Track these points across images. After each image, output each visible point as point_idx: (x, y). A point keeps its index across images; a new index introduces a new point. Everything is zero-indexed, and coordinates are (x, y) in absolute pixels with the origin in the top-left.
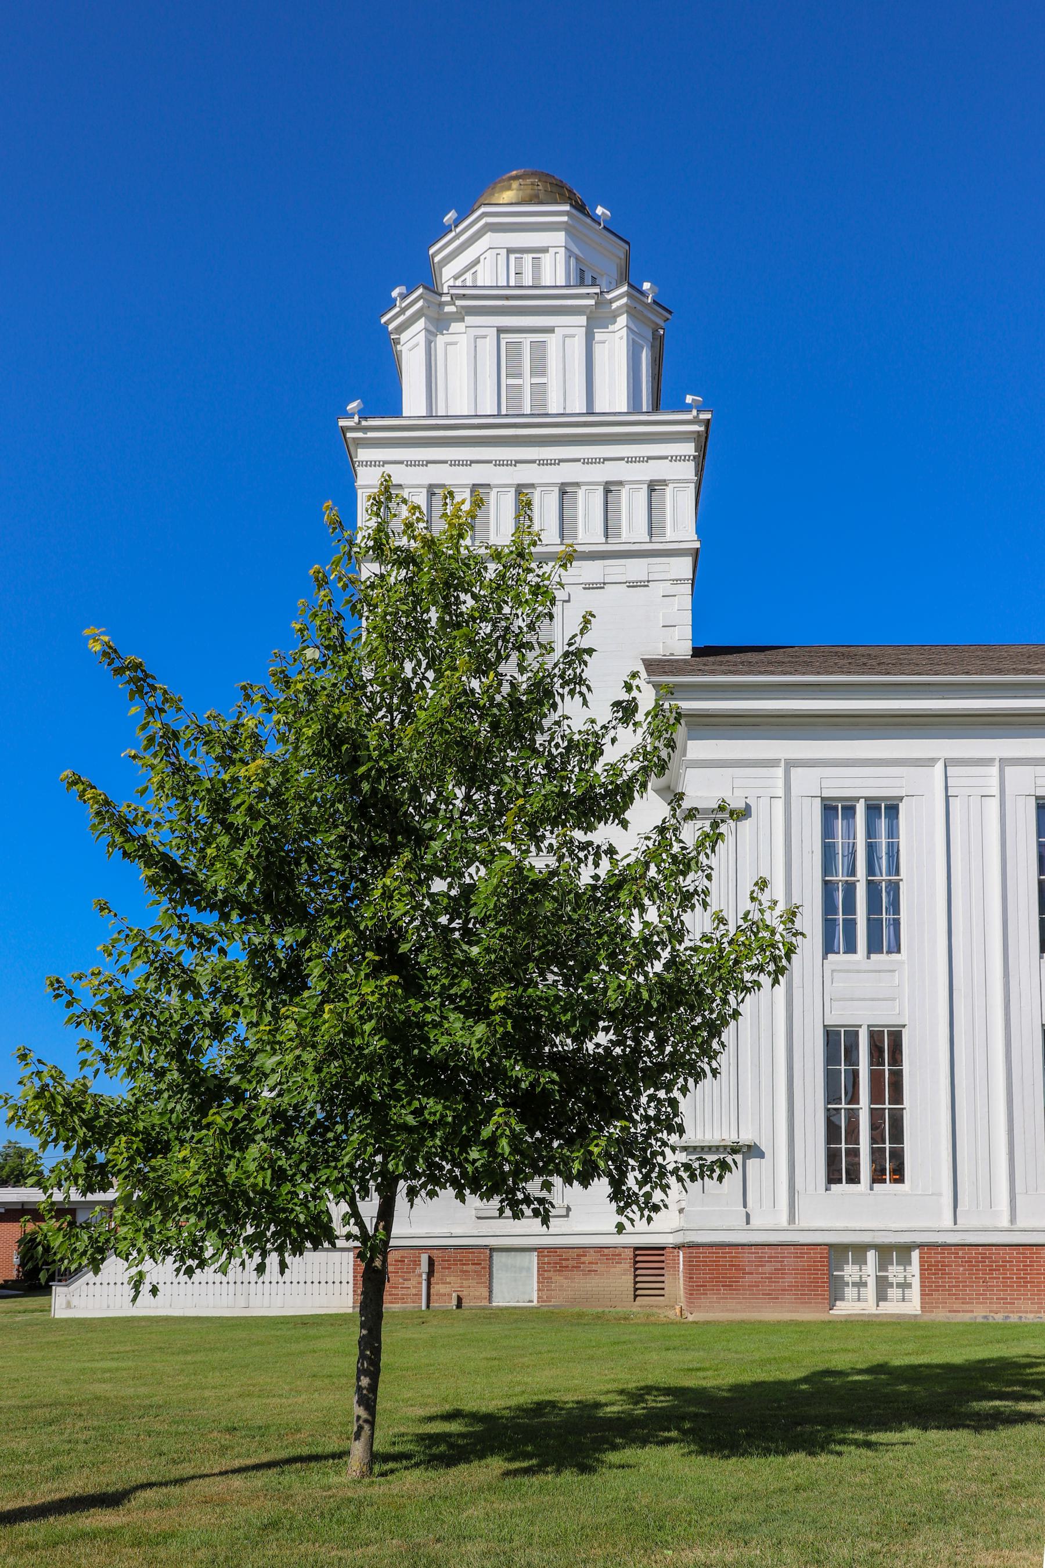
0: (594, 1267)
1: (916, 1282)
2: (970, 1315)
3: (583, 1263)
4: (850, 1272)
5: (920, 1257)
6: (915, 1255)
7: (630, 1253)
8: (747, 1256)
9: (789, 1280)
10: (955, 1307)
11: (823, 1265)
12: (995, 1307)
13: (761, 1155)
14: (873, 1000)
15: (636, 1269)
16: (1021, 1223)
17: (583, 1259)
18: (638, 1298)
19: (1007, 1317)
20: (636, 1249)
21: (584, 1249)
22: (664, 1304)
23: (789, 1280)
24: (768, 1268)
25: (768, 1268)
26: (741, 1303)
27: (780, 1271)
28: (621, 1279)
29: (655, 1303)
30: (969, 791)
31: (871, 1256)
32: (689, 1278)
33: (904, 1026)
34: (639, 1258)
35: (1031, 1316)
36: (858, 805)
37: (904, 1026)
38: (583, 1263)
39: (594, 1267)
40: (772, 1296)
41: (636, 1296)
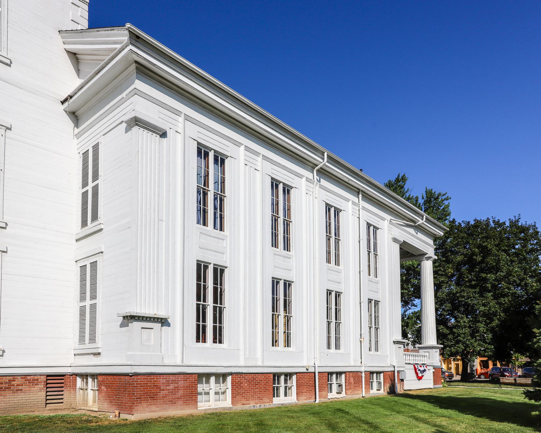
0: (20, 387)
1: (229, 393)
2: (249, 406)
3: (13, 385)
4: (201, 388)
5: (232, 380)
6: (229, 379)
7: (43, 378)
8: (162, 380)
9: (181, 393)
10: (244, 402)
11: (189, 383)
12: (257, 401)
13: (169, 325)
14: (215, 252)
15: (47, 388)
16: (186, 363)
17: (13, 383)
18: (47, 405)
19: (260, 406)
20: (48, 376)
21: (14, 376)
22: (63, 407)
23: (181, 393)
24: (171, 387)
25: (171, 387)
26: (158, 407)
27: (177, 389)
28: (38, 394)
29: (58, 408)
30: (252, 165)
31: (213, 379)
32: (233, 397)
33: (226, 267)
34: (48, 381)
35: (267, 404)
36: (210, 153)
37: (226, 267)
38: (13, 385)
39: (20, 387)
40: (173, 402)
41: (46, 404)
